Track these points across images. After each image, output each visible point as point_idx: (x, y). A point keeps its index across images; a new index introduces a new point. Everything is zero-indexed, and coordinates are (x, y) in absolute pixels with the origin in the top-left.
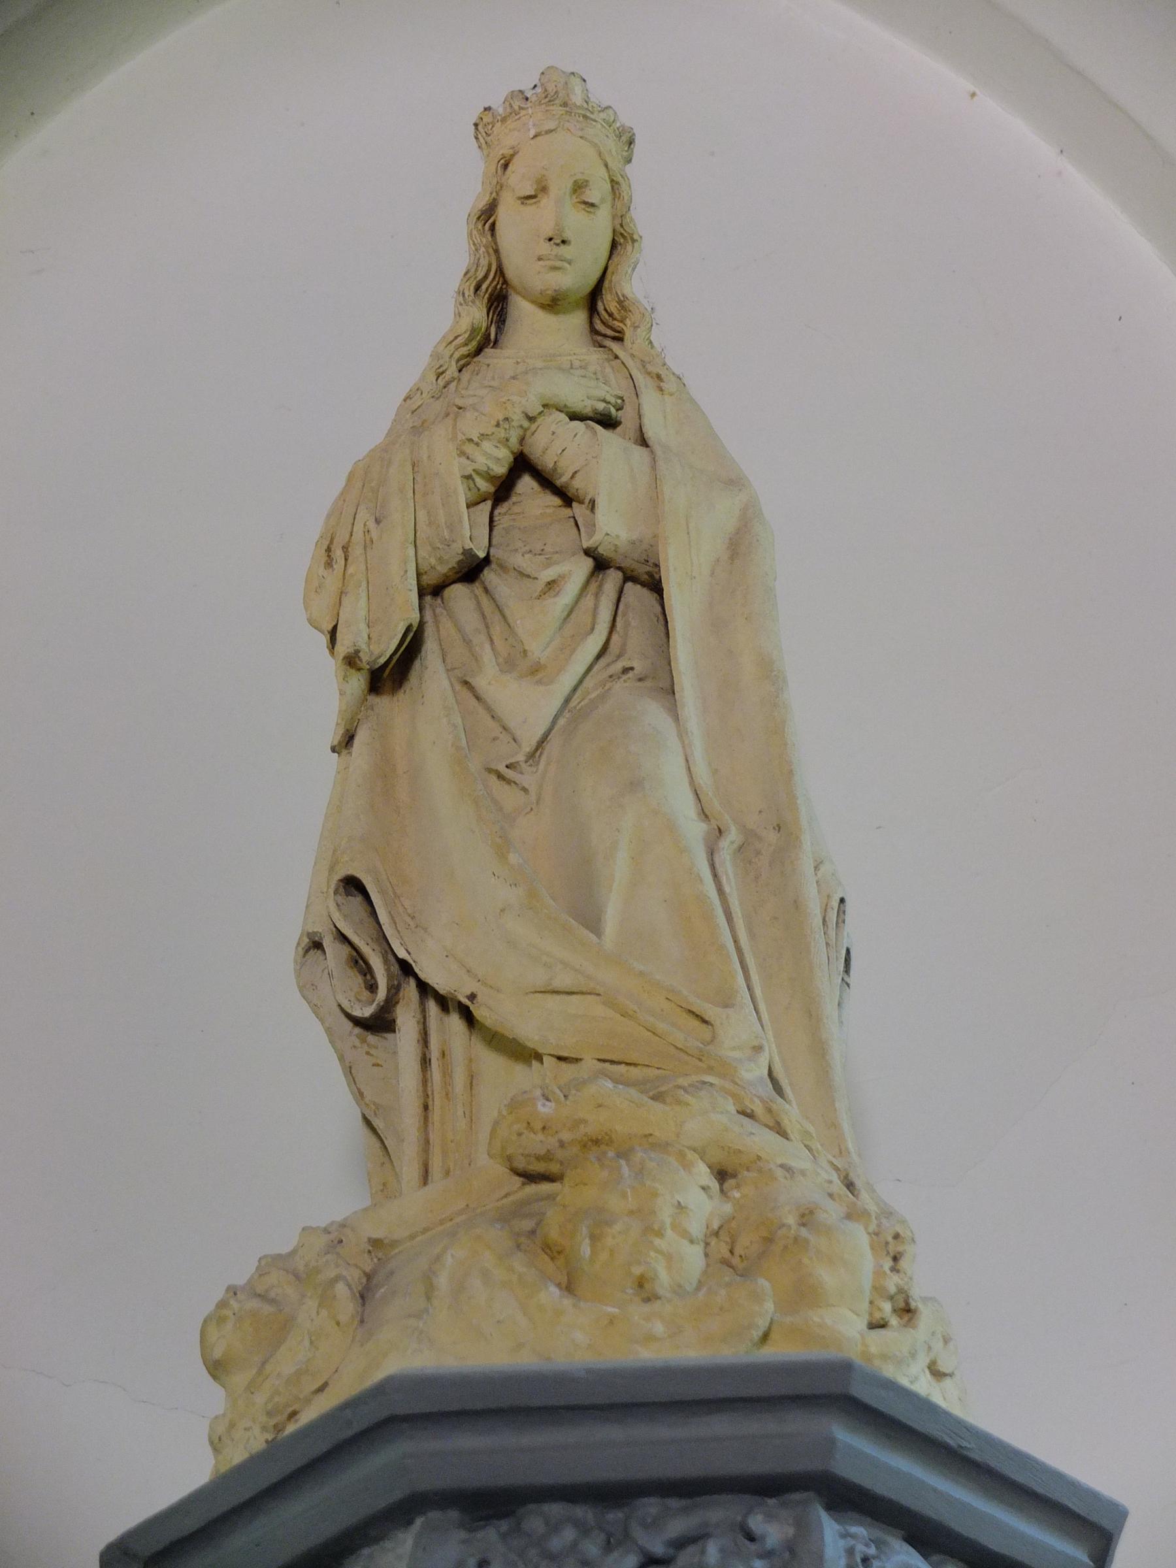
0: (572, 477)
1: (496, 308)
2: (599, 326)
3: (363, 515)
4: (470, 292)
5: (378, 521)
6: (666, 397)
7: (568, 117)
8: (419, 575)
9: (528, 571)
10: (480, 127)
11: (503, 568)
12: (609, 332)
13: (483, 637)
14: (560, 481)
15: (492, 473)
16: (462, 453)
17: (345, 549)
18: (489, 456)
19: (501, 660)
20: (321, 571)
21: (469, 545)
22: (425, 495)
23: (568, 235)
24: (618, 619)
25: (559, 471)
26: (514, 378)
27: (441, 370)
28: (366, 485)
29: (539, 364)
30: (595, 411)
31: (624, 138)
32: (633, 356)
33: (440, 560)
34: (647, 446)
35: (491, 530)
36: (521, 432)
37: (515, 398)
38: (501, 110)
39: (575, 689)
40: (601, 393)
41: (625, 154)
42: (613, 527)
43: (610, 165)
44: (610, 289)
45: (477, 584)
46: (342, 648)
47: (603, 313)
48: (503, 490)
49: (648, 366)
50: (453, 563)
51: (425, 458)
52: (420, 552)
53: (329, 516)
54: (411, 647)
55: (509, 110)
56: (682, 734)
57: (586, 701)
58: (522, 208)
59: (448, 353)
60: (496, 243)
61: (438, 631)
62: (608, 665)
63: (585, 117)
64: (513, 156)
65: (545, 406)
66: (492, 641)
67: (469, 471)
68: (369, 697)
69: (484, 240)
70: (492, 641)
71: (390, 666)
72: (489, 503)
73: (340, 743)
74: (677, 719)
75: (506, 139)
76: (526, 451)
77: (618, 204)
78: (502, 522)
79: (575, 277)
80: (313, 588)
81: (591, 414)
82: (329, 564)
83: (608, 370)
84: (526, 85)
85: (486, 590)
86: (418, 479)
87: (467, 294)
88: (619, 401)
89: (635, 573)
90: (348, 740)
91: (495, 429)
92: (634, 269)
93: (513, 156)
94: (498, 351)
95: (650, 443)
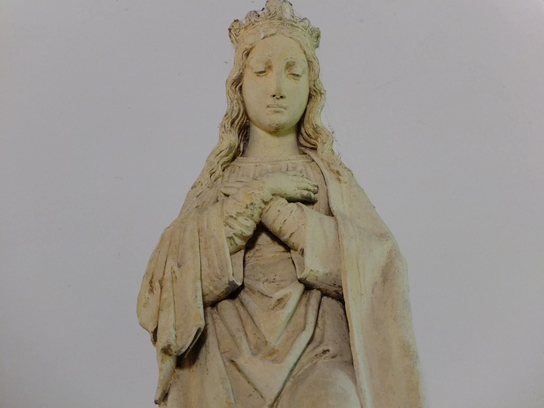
0: (290, 236)
1: (243, 133)
2: (302, 142)
3: (171, 263)
4: (228, 126)
5: (179, 266)
6: (342, 184)
7: (282, 26)
8: (203, 296)
9: (267, 293)
10: (232, 31)
11: (252, 290)
12: (308, 145)
13: (242, 334)
14: (284, 238)
15: (244, 235)
16: (227, 224)
17: (161, 282)
18: (242, 225)
19: (252, 347)
20: (147, 295)
21: (232, 279)
22: (206, 249)
23: (284, 93)
24: (319, 319)
25: (282, 232)
26: (255, 179)
27: (213, 171)
28: (171, 245)
29: (269, 167)
30: (302, 196)
31: (314, 35)
32: (322, 160)
33: (216, 288)
34: (333, 216)
35: (244, 266)
36: (260, 210)
37: (256, 192)
38: (244, 22)
39: (295, 364)
40: (306, 185)
41: (315, 43)
42: (315, 266)
43: (307, 52)
44: (309, 121)
45: (237, 300)
46: (162, 342)
47: (305, 134)
48: (250, 243)
49: (331, 166)
50: (223, 289)
51: (206, 226)
52: (204, 283)
53: (151, 261)
54: (200, 340)
55: (248, 22)
56: (359, 392)
57: (302, 370)
58: (257, 78)
59: (216, 161)
60: (242, 97)
61: (215, 328)
62: (315, 348)
63: (292, 25)
64: (251, 49)
65: (273, 195)
66: (246, 335)
67: (231, 234)
68: (176, 370)
69: (236, 96)
70: (246, 335)
71: (189, 351)
72: (243, 251)
73: (160, 399)
74: (355, 381)
75: (247, 39)
76: (263, 221)
77: (312, 74)
78: (251, 262)
79: (288, 116)
80: (142, 304)
81: (300, 198)
82: (151, 291)
83: (309, 169)
84: (258, 9)
85: (242, 304)
86: (202, 239)
87: (226, 126)
88: (316, 188)
89: (328, 292)
90: (165, 396)
91: (245, 210)
92: (322, 109)
93: (251, 49)
94: (245, 158)
95: (334, 214)
